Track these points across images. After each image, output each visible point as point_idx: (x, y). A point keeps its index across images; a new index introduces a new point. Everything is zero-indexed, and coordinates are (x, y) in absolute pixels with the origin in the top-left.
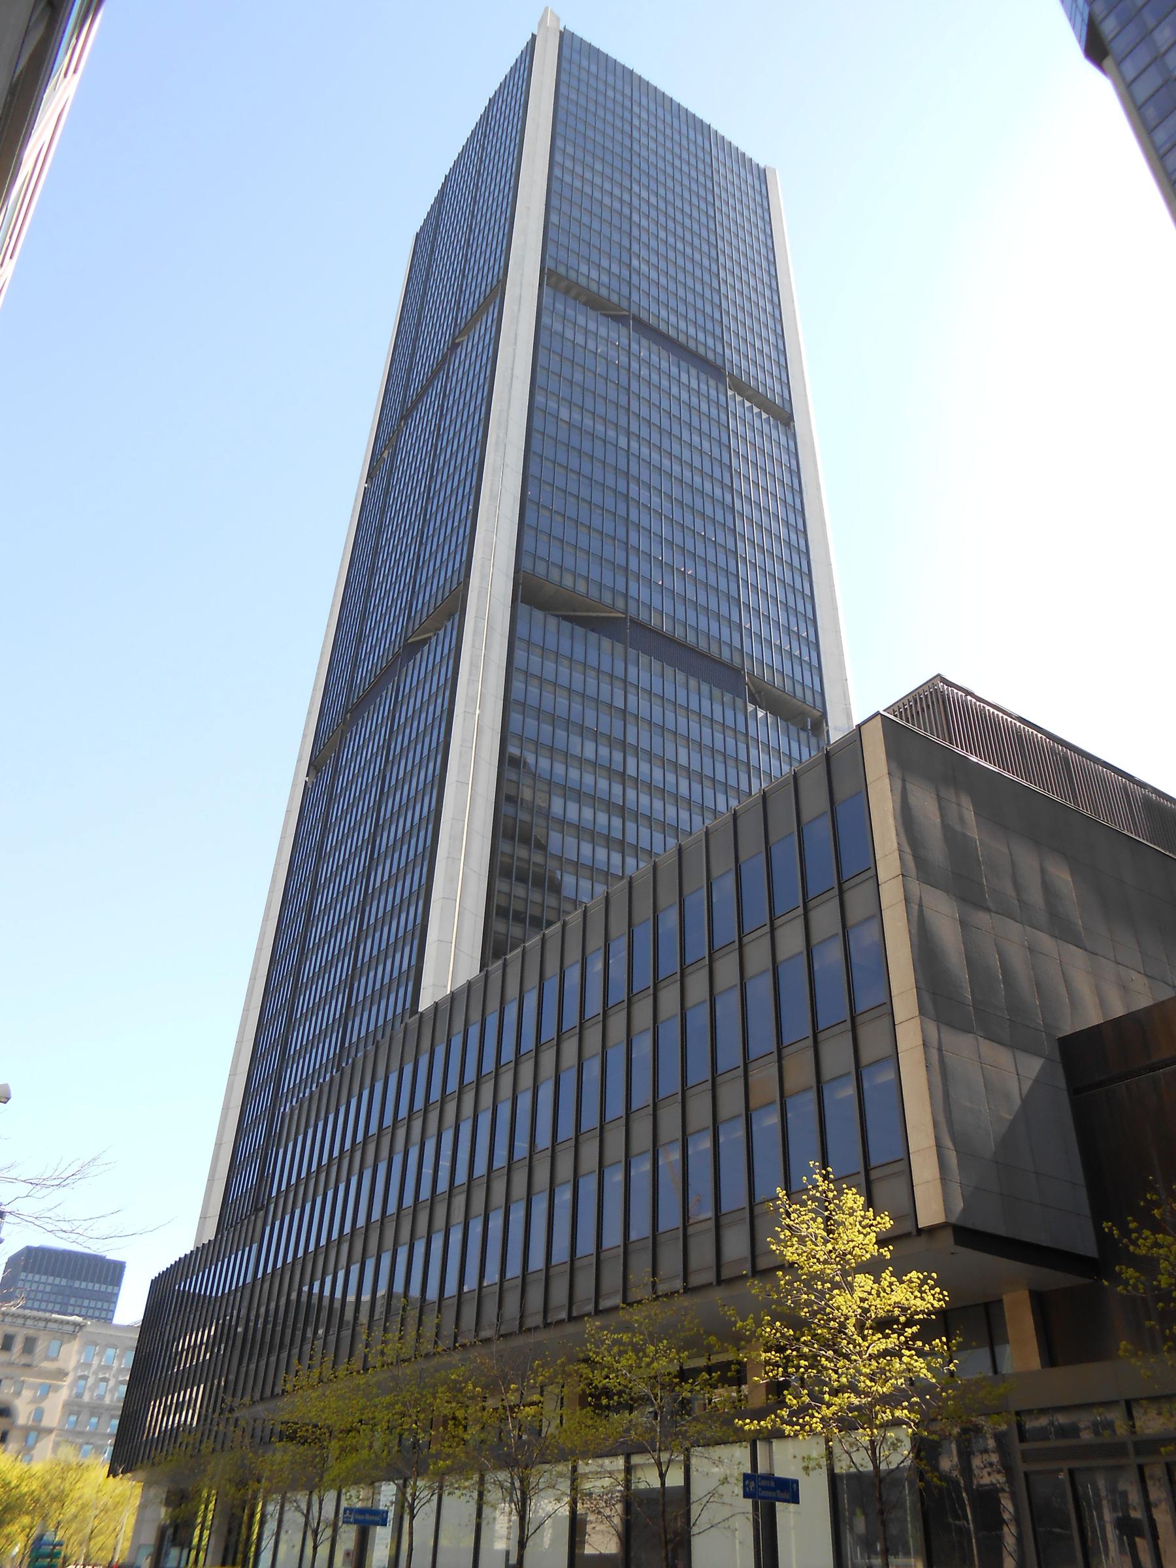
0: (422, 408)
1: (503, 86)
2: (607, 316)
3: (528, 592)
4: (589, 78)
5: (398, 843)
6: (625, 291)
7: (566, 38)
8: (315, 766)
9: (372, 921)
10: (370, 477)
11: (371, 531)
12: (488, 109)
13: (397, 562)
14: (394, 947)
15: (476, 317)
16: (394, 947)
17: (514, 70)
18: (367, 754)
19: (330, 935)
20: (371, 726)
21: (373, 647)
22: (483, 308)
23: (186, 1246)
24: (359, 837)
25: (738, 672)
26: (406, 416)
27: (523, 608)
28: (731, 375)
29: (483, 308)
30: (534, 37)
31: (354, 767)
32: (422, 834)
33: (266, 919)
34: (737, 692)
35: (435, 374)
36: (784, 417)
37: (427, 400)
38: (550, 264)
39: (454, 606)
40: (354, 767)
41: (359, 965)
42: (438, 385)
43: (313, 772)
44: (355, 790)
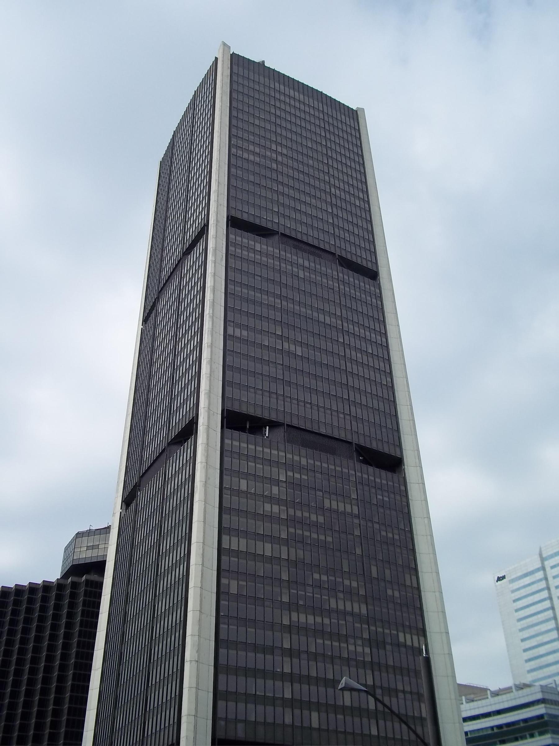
5: (176, 491)
8: (145, 320)
9: (169, 494)
11: (157, 260)
14: (176, 565)
16: (176, 565)
18: (163, 381)
21: (168, 261)
25: (341, 265)
26: (160, 291)
27: (228, 432)
30: (216, 59)
31: (157, 389)
32: (188, 468)
34: (341, 257)
40: (157, 389)
41: (164, 515)
42: (175, 282)
43: (124, 507)
44: (161, 371)
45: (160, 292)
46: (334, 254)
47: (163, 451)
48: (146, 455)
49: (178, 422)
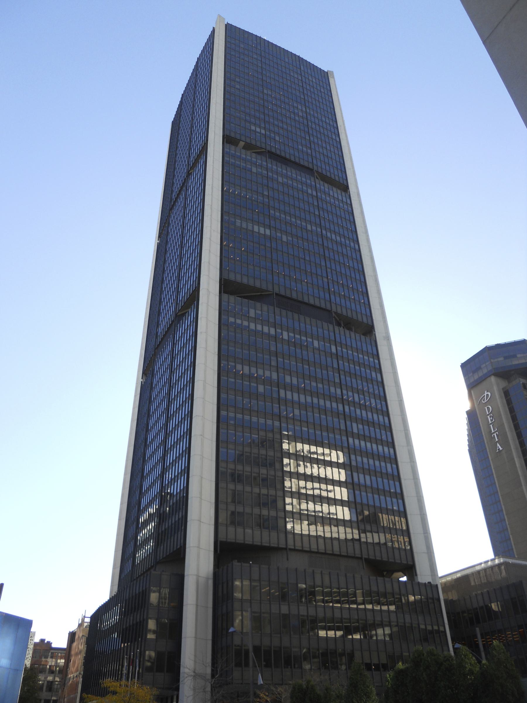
0: (177, 204)
1: (203, 51)
2: (245, 297)
3: (226, 287)
4: (241, 45)
6: (263, 140)
7: (229, 28)
10: (159, 237)
12: (197, 63)
13: (177, 233)
15: (196, 161)
17: (206, 44)
19: (155, 437)
20: (165, 355)
22: (199, 156)
23: (105, 597)
24: (166, 365)
27: (225, 296)
28: (317, 172)
29: (199, 156)
32: (189, 372)
33: (150, 280)
35: (182, 188)
36: (345, 188)
37: (179, 201)
38: (227, 133)
39: (194, 298)
45: (171, 209)
46: (329, 311)
47: (173, 322)
48: (160, 330)
49: (183, 295)
